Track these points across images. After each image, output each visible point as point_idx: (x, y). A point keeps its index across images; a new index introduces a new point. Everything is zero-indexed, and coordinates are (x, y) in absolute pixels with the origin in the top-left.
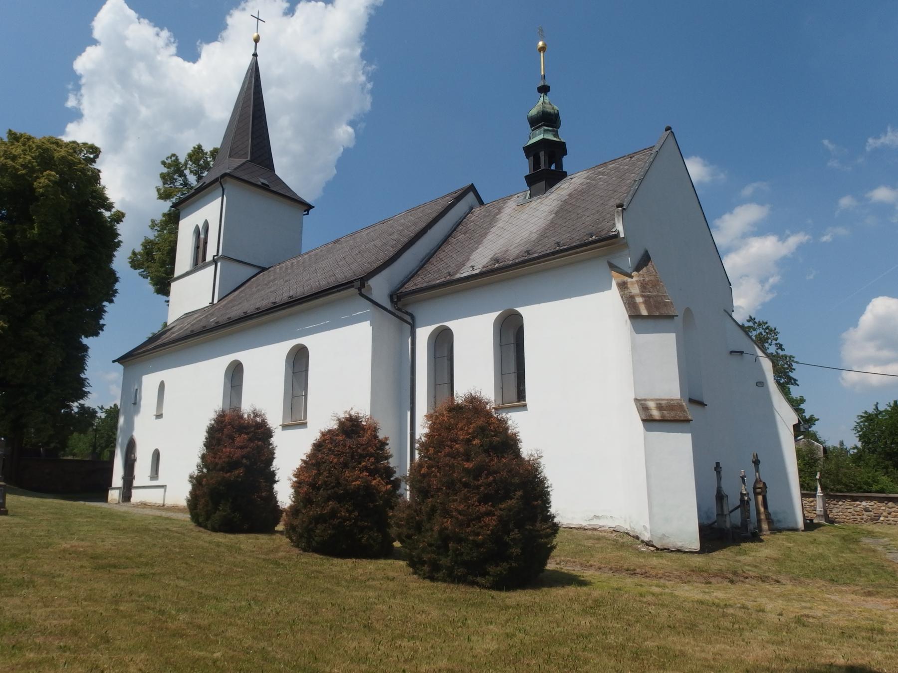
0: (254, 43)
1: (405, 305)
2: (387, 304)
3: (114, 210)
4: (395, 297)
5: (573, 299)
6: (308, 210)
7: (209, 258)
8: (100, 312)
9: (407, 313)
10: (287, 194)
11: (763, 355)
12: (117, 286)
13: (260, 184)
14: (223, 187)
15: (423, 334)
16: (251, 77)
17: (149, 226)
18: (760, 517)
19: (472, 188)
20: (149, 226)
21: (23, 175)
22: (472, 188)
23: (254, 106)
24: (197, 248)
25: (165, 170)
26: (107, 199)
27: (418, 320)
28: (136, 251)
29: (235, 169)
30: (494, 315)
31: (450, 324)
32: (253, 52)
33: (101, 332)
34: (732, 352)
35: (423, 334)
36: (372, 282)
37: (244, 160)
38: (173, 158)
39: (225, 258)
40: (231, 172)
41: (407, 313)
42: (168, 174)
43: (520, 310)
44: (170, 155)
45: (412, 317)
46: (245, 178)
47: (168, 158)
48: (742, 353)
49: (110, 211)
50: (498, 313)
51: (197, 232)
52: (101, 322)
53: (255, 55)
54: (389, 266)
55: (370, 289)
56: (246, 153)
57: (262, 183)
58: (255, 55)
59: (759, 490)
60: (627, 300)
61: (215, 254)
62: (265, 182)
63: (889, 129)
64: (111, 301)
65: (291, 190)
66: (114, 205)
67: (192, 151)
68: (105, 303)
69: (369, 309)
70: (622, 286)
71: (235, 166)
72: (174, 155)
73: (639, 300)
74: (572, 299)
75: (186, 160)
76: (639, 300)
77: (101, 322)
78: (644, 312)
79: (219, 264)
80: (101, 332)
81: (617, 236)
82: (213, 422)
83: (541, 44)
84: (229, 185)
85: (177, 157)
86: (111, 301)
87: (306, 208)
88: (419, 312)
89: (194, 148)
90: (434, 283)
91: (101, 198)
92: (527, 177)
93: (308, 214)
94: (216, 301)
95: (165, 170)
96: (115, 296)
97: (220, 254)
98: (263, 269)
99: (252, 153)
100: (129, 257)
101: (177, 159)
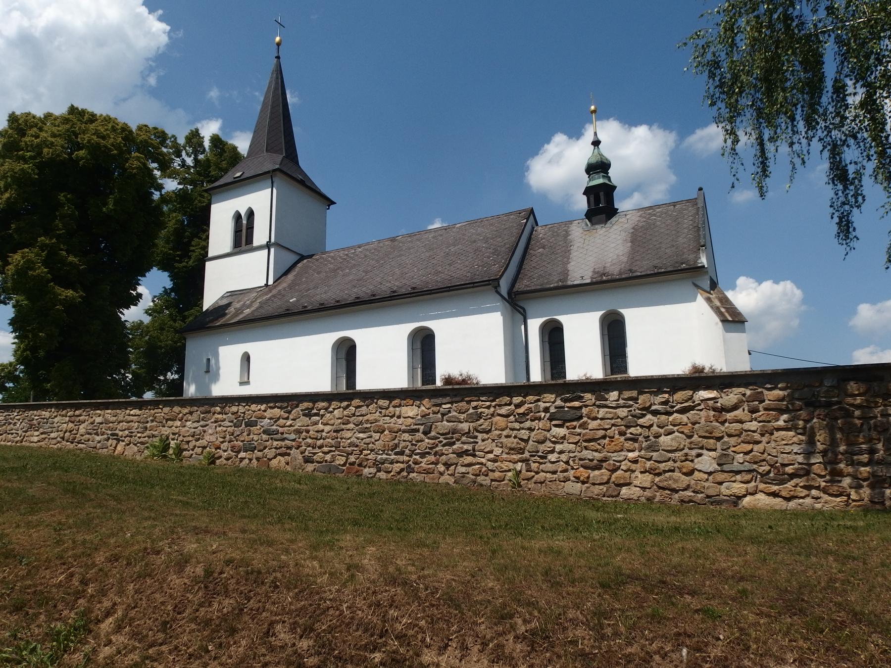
6: (329, 206)
7: (256, 243)
9: (521, 307)
15: (534, 325)
21: (114, 155)
27: (529, 311)
39: (277, 245)
43: (623, 311)
45: (524, 310)
51: (238, 217)
53: (278, 57)
63: (160, 12)
70: (709, 300)
73: (723, 310)
76: (723, 310)
78: (730, 319)
79: (272, 250)
81: (703, 267)
82: (475, 382)
83: (593, 108)
88: (530, 307)
90: (548, 286)
94: (271, 282)
97: (273, 240)
98: (302, 258)
99: (286, 150)
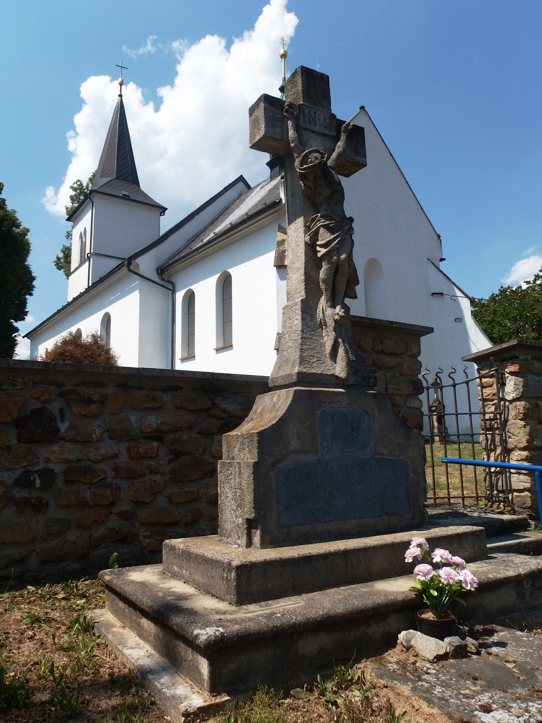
0: (120, 86)
1: (170, 276)
2: (156, 278)
3: (21, 227)
4: (159, 270)
5: (259, 258)
6: (164, 212)
8: (24, 303)
10: (145, 201)
11: (462, 295)
12: (34, 283)
13: (121, 195)
14: (92, 202)
16: (117, 113)
17: (66, 236)
18: (433, 430)
19: (241, 179)
20: (66, 236)
22: (241, 179)
23: (119, 135)
24: (81, 249)
25: (73, 193)
26: (17, 219)
27: (178, 286)
28: (59, 256)
29: (102, 186)
30: (217, 276)
31: (191, 287)
32: (119, 93)
33: (25, 317)
34: (433, 294)
35: (180, 296)
36: (140, 260)
37: (111, 179)
38: (79, 183)
40: (97, 189)
41: (168, 281)
42: (75, 195)
43: (229, 270)
44: (75, 181)
45: (173, 284)
46: (109, 192)
47: (74, 183)
48: (442, 294)
49: (19, 228)
50: (217, 276)
52: (26, 310)
53: (120, 96)
54: (155, 247)
55: (138, 265)
56: (113, 173)
57: (123, 195)
58: (120, 96)
59: (433, 408)
60: (278, 254)
61: (89, 252)
62: (127, 193)
64: (31, 295)
65: (150, 198)
66: (22, 224)
67: (92, 176)
68: (27, 297)
69: (136, 281)
71: (102, 184)
72: (79, 181)
74: (259, 258)
75: (88, 184)
77: (26, 310)
79: (91, 259)
80: (25, 317)
84: (97, 198)
85: (81, 182)
86: (31, 295)
87: (162, 210)
89: (93, 173)
91: (10, 220)
92: (268, 164)
93: (164, 215)
95: (73, 193)
96: (33, 290)
97: (92, 251)
99: (117, 172)
100: (54, 261)
101: (81, 184)
